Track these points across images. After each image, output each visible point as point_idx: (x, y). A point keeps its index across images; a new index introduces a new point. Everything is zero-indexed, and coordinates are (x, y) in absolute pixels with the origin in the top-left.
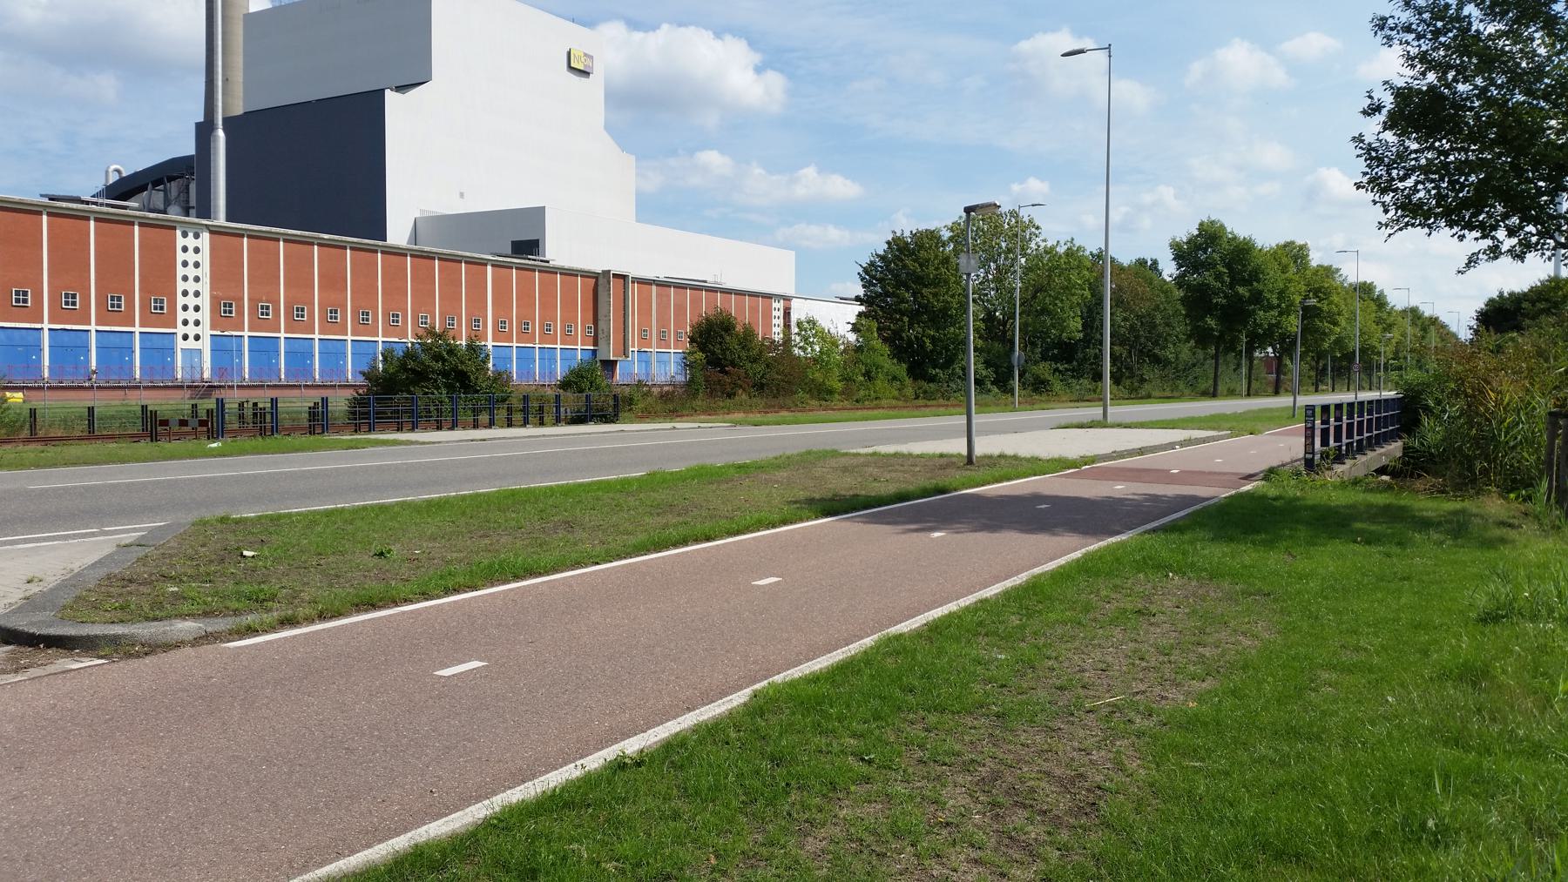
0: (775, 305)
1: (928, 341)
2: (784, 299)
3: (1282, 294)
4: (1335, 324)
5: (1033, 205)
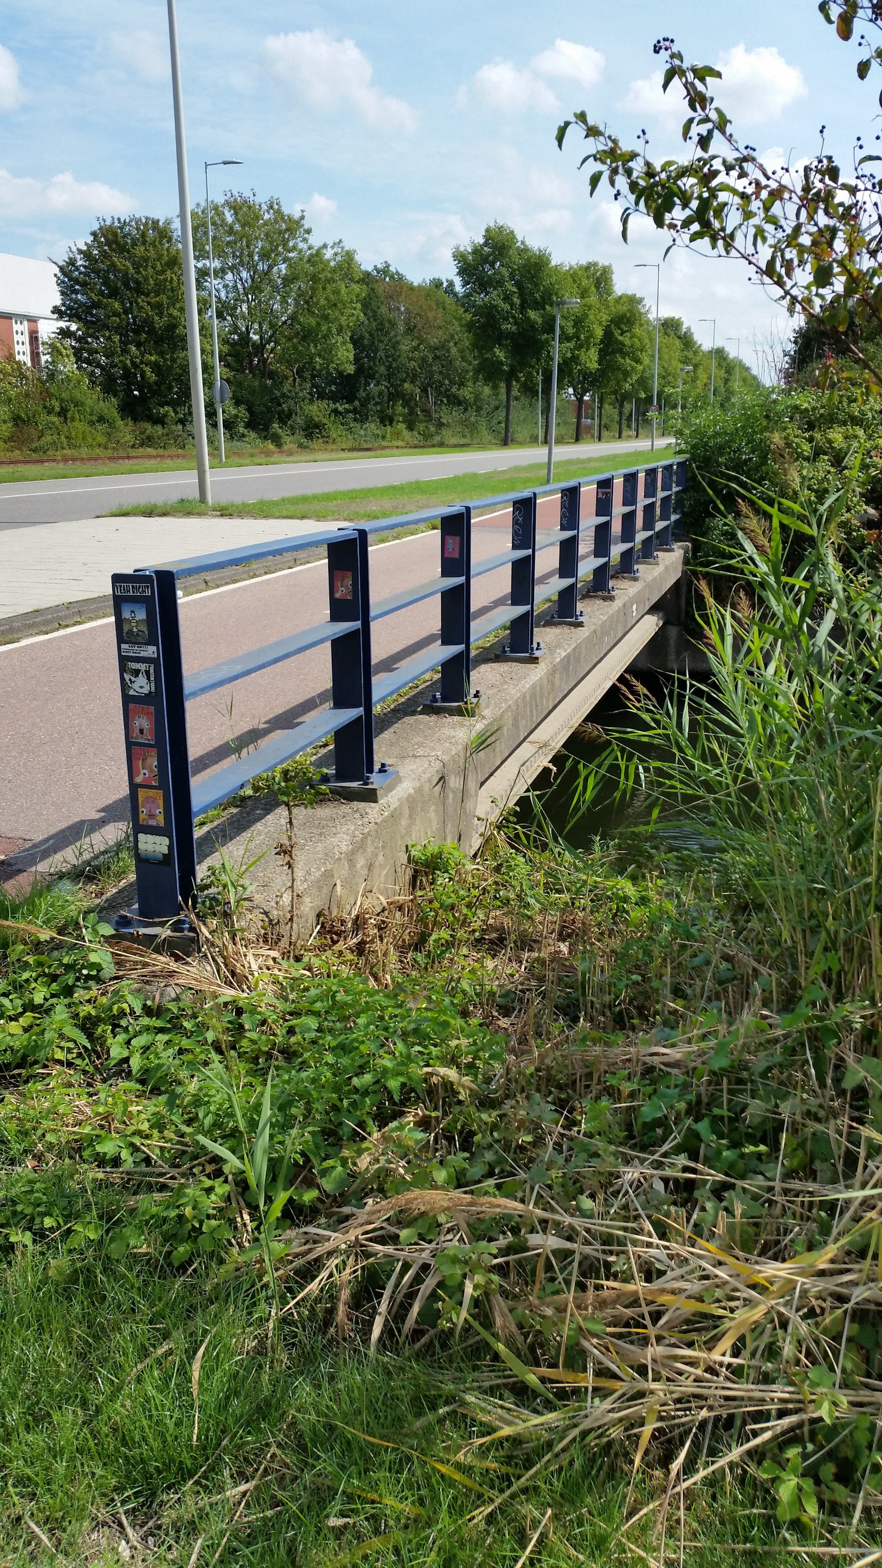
0: (17, 327)
1: (148, 369)
2: (29, 321)
3: (579, 322)
4: (638, 361)
5: (225, 163)
